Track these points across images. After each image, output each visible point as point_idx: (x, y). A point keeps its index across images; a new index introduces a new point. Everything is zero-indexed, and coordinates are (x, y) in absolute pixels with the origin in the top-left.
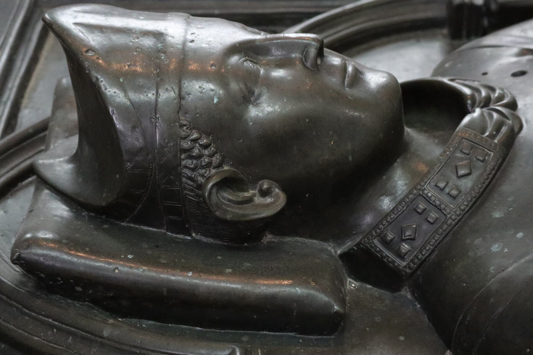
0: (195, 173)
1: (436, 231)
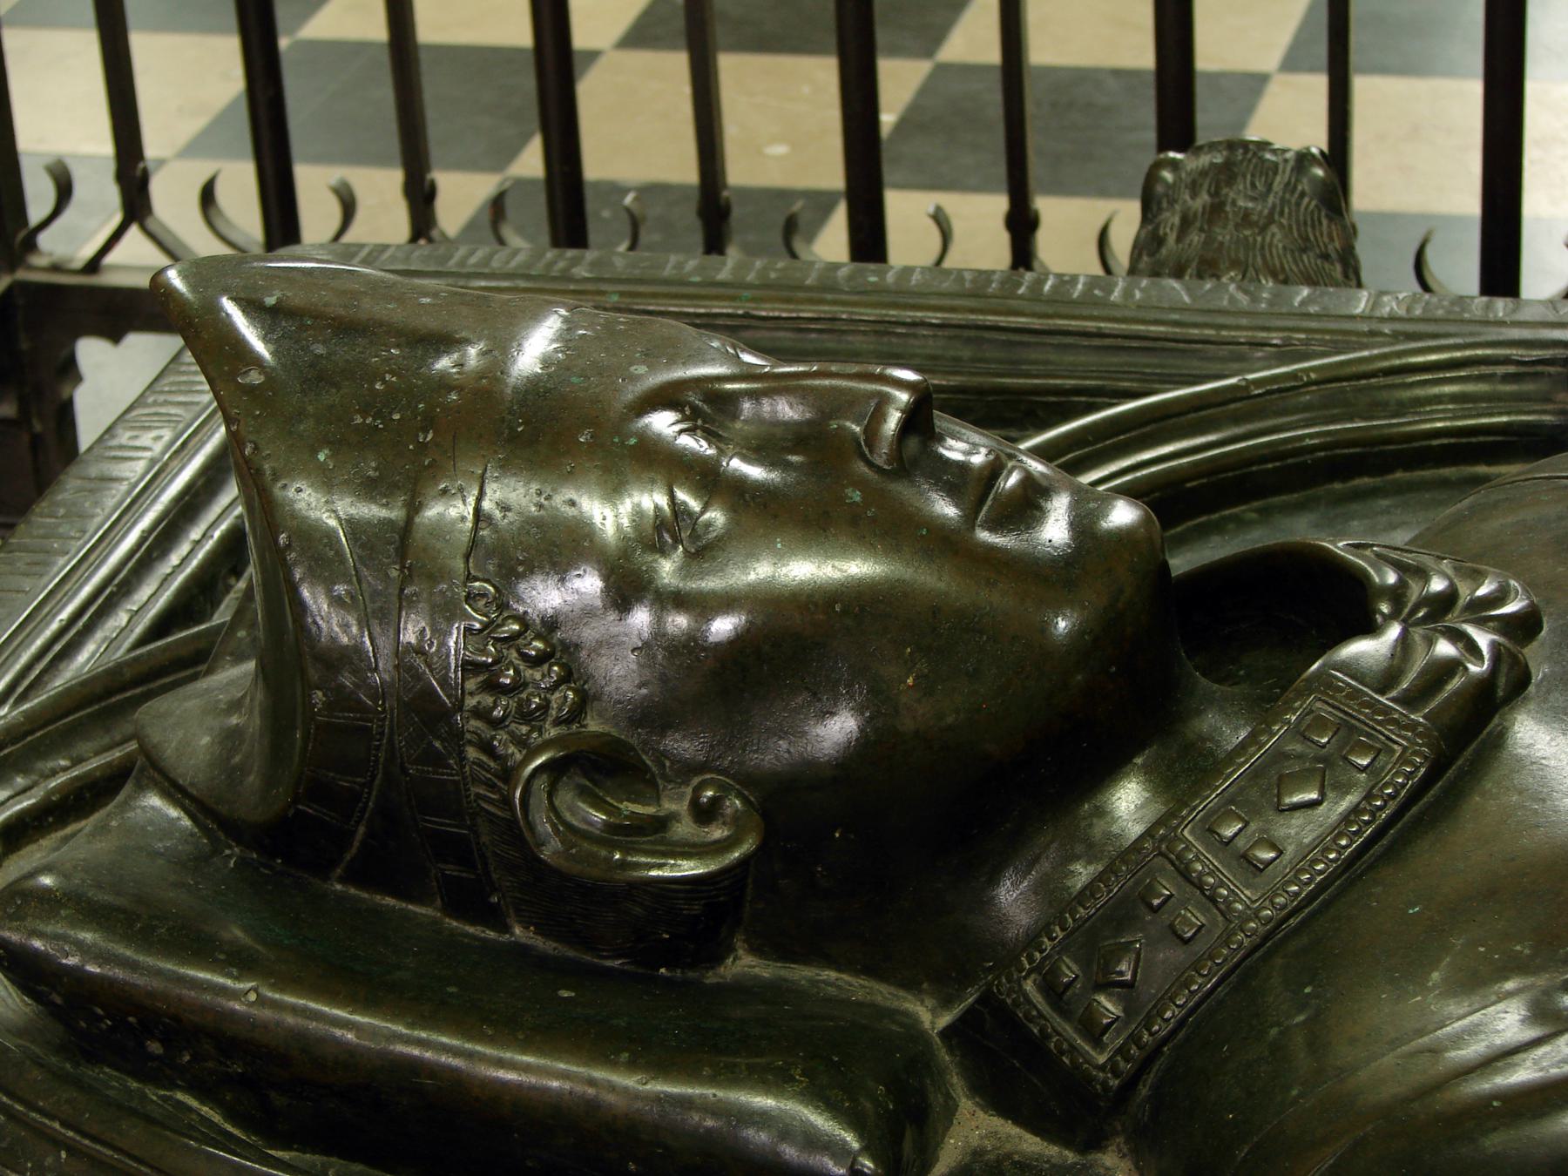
0: (502, 735)
1: (1196, 966)
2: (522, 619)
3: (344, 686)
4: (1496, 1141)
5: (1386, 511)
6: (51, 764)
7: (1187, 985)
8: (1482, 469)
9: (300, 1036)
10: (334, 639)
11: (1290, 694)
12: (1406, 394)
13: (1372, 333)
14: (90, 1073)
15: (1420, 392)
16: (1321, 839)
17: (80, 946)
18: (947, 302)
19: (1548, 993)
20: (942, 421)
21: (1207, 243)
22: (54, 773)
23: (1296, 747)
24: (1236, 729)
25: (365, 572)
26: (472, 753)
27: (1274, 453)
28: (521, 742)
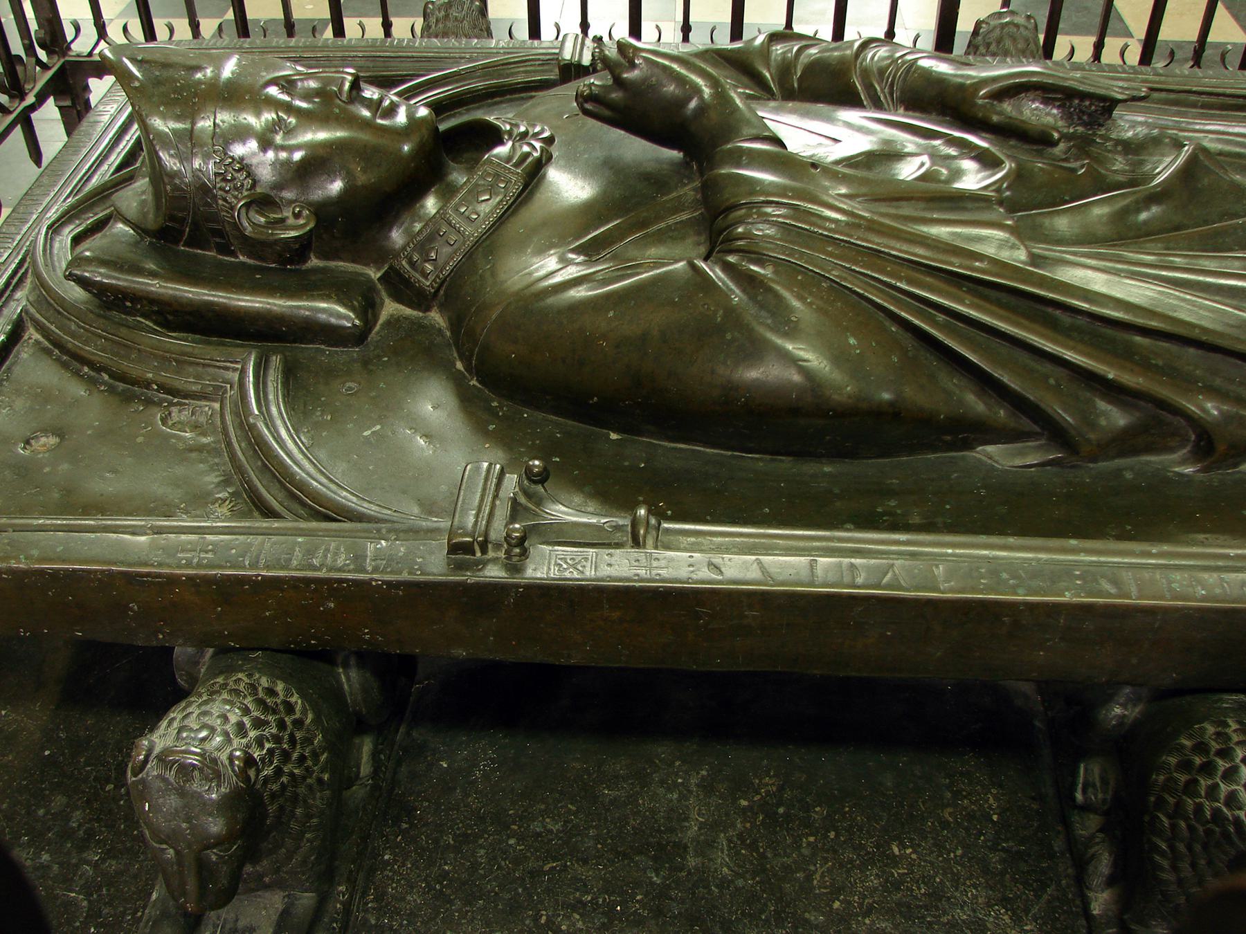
1: (455, 253)
2: (232, 158)
3: (176, 184)
4: (551, 300)
5: (505, 108)
6: (87, 216)
7: (453, 259)
8: (533, 94)
9: (175, 297)
10: (172, 169)
11: (479, 166)
12: (508, 72)
13: (497, 53)
14: (108, 313)
15: (512, 71)
16: (492, 210)
17: (101, 274)
18: (364, 49)
19: (564, 254)
20: (363, 85)
21: (445, 26)
22: (88, 219)
23: (482, 182)
24: (463, 178)
25: (179, 146)
26: (220, 202)
27: (469, 92)
28: (236, 197)
